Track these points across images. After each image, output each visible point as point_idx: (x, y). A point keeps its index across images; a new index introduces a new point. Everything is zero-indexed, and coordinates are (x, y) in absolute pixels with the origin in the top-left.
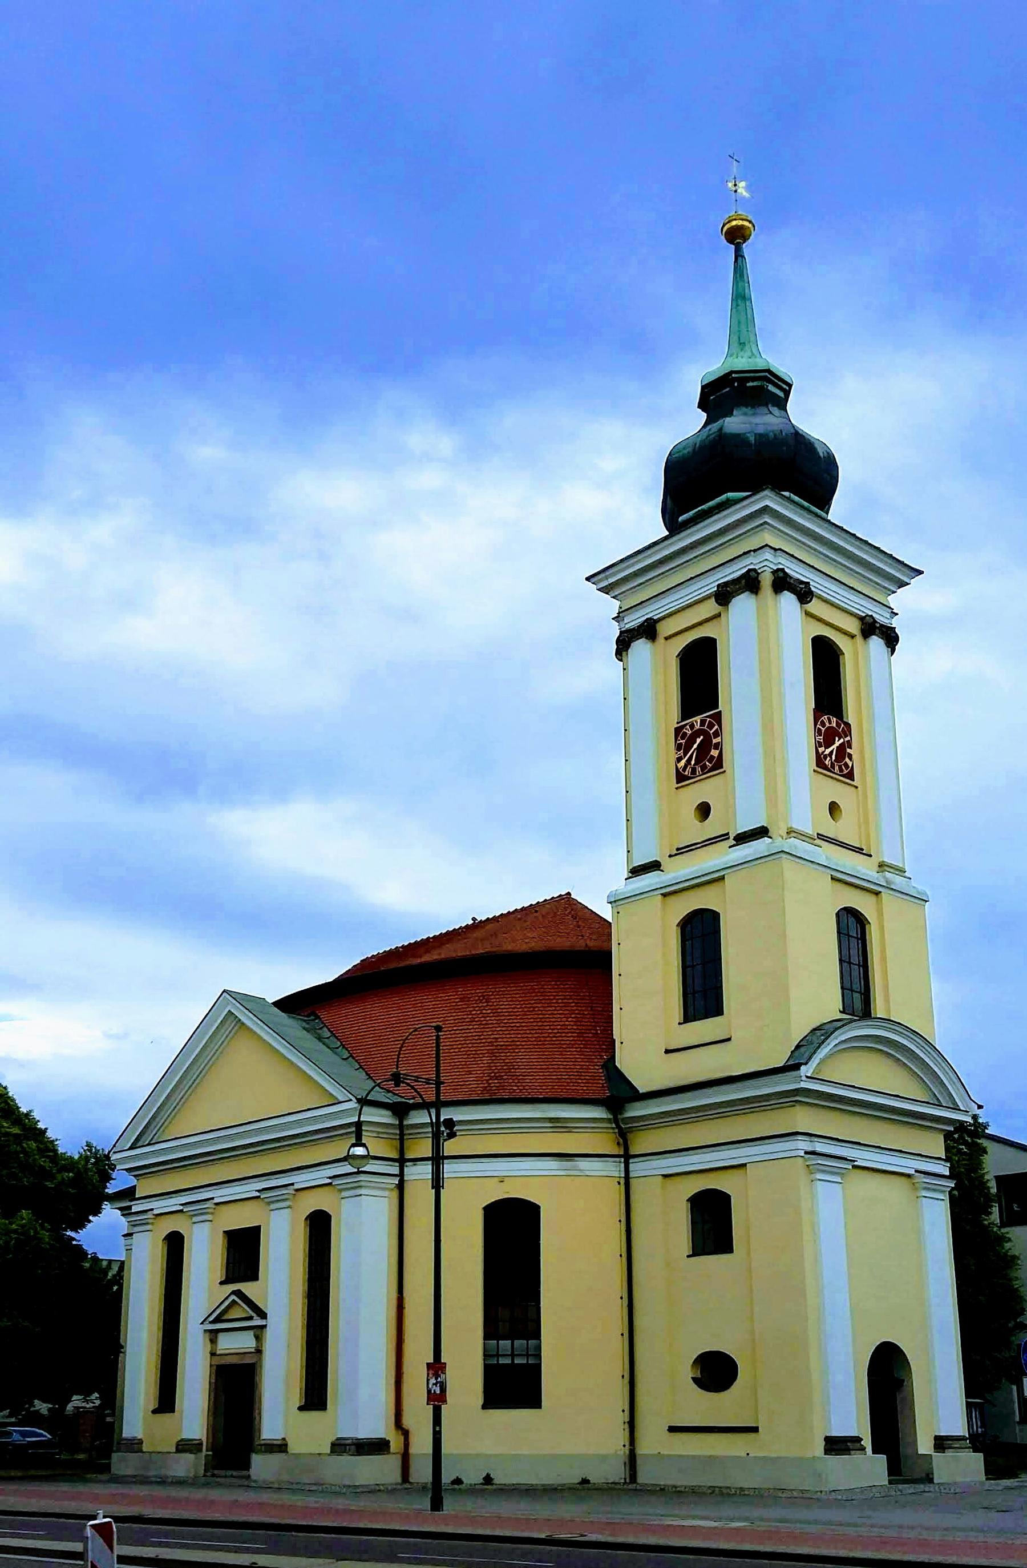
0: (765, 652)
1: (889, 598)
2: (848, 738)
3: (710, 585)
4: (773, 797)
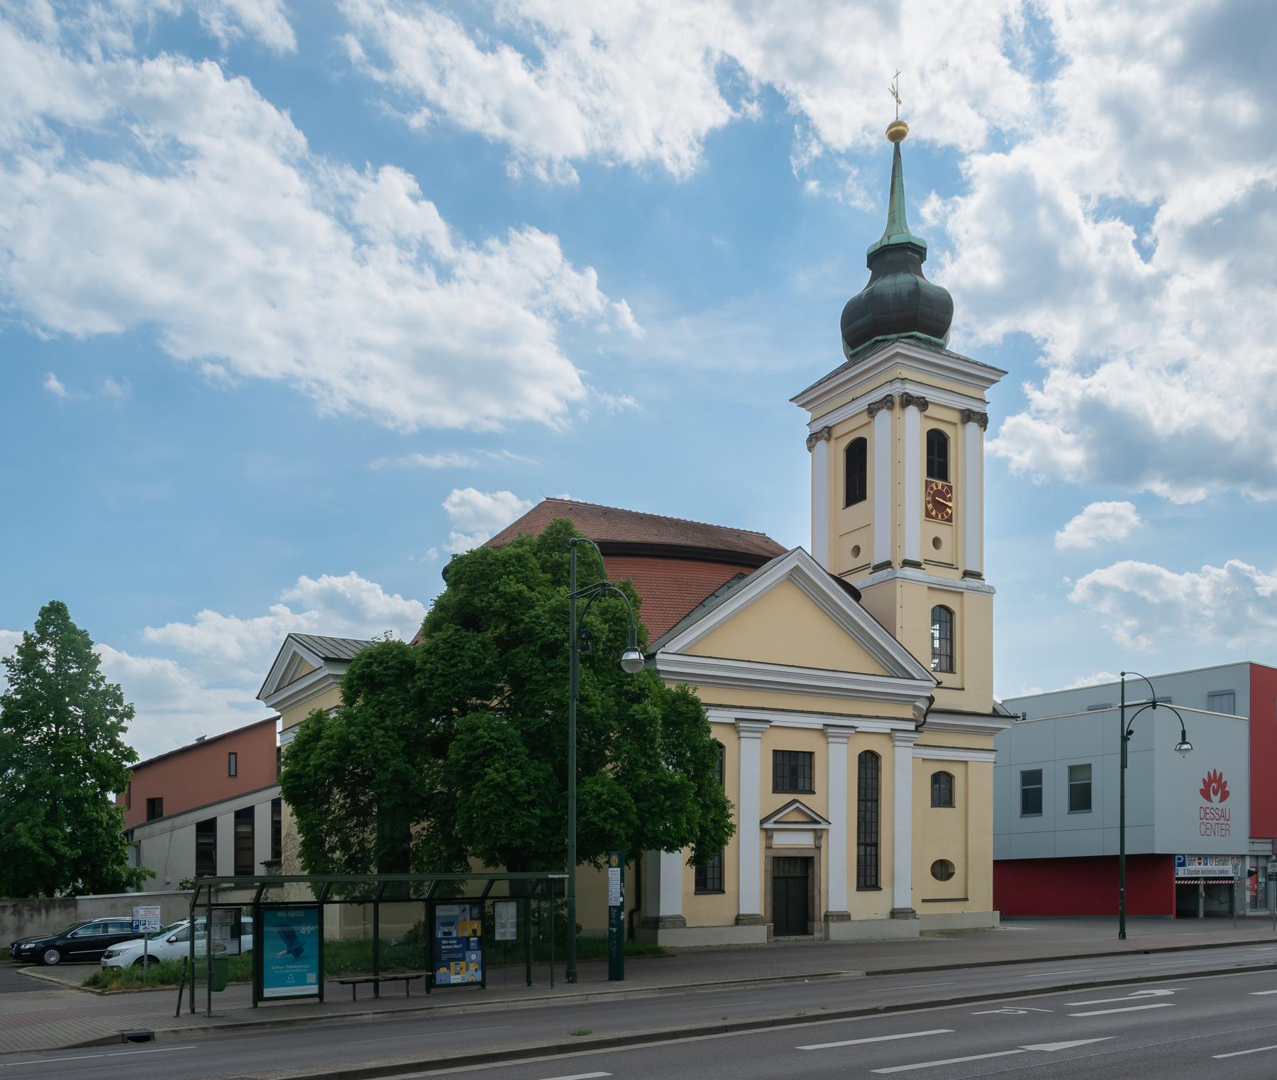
0: (898, 448)
3: (863, 404)
4: (896, 545)
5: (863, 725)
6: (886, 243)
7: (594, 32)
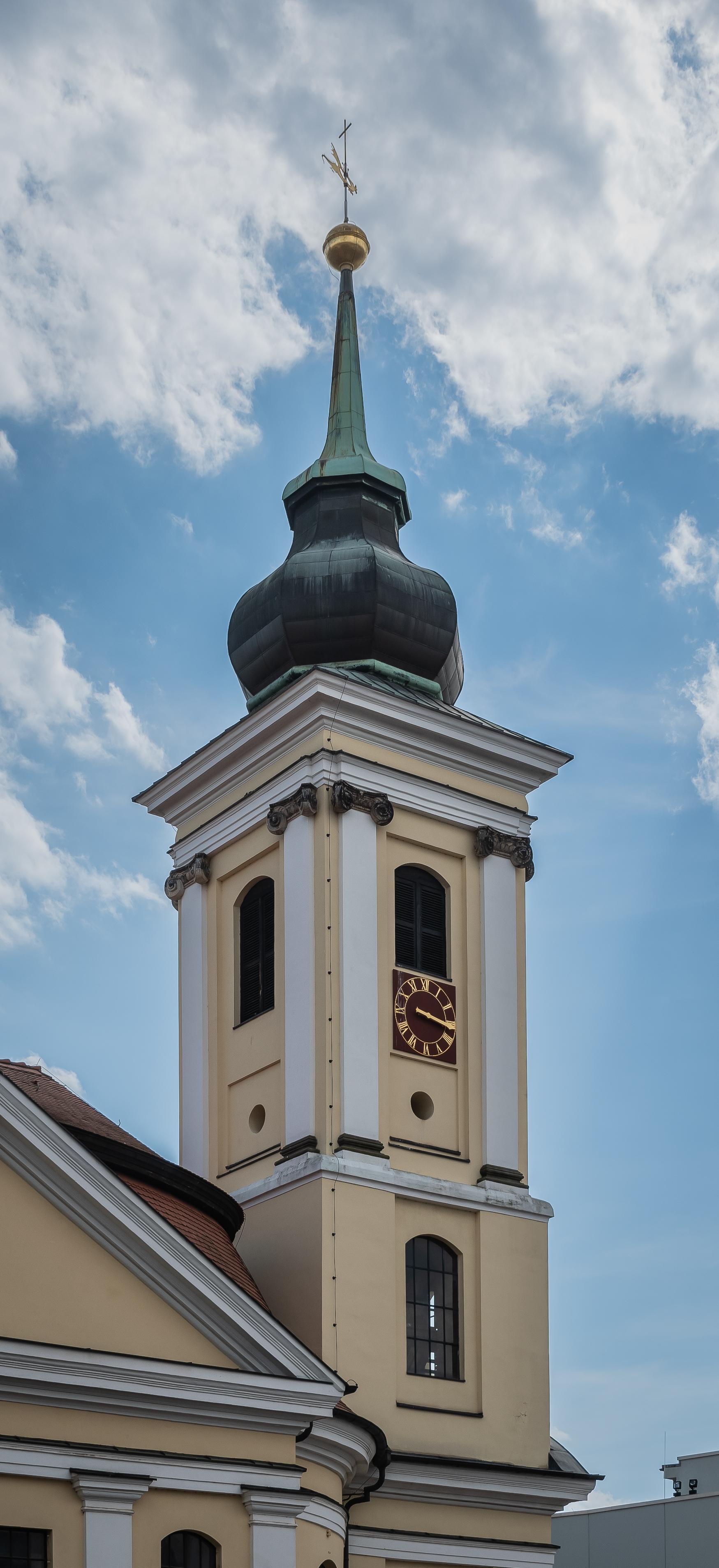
0: (336, 893)
1: (529, 797)
2: (449, 1006)
3: (257, 810)
4: (327, 1100)
5: (167, 1474)
6: (316, 474)
7: (27, 165)
